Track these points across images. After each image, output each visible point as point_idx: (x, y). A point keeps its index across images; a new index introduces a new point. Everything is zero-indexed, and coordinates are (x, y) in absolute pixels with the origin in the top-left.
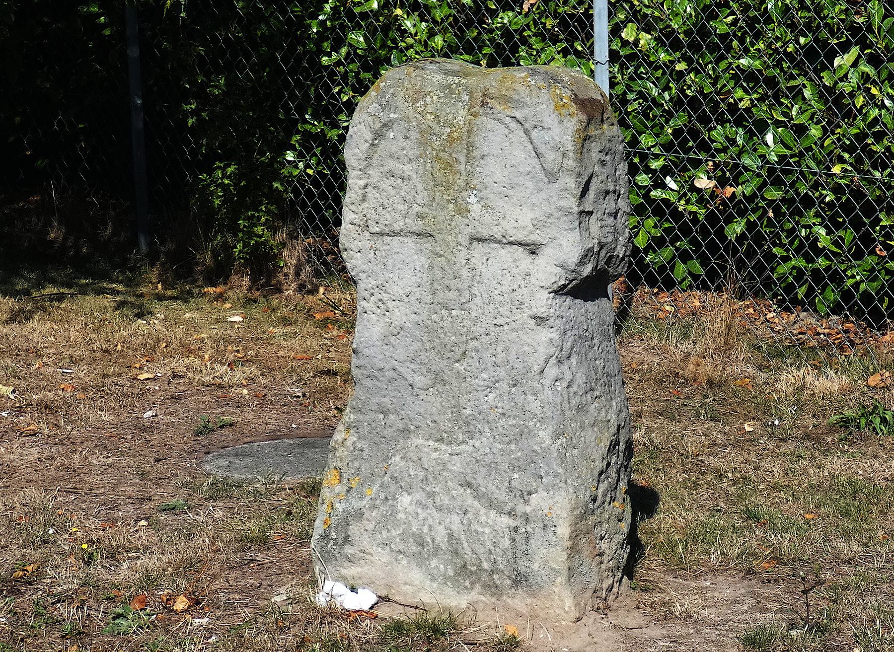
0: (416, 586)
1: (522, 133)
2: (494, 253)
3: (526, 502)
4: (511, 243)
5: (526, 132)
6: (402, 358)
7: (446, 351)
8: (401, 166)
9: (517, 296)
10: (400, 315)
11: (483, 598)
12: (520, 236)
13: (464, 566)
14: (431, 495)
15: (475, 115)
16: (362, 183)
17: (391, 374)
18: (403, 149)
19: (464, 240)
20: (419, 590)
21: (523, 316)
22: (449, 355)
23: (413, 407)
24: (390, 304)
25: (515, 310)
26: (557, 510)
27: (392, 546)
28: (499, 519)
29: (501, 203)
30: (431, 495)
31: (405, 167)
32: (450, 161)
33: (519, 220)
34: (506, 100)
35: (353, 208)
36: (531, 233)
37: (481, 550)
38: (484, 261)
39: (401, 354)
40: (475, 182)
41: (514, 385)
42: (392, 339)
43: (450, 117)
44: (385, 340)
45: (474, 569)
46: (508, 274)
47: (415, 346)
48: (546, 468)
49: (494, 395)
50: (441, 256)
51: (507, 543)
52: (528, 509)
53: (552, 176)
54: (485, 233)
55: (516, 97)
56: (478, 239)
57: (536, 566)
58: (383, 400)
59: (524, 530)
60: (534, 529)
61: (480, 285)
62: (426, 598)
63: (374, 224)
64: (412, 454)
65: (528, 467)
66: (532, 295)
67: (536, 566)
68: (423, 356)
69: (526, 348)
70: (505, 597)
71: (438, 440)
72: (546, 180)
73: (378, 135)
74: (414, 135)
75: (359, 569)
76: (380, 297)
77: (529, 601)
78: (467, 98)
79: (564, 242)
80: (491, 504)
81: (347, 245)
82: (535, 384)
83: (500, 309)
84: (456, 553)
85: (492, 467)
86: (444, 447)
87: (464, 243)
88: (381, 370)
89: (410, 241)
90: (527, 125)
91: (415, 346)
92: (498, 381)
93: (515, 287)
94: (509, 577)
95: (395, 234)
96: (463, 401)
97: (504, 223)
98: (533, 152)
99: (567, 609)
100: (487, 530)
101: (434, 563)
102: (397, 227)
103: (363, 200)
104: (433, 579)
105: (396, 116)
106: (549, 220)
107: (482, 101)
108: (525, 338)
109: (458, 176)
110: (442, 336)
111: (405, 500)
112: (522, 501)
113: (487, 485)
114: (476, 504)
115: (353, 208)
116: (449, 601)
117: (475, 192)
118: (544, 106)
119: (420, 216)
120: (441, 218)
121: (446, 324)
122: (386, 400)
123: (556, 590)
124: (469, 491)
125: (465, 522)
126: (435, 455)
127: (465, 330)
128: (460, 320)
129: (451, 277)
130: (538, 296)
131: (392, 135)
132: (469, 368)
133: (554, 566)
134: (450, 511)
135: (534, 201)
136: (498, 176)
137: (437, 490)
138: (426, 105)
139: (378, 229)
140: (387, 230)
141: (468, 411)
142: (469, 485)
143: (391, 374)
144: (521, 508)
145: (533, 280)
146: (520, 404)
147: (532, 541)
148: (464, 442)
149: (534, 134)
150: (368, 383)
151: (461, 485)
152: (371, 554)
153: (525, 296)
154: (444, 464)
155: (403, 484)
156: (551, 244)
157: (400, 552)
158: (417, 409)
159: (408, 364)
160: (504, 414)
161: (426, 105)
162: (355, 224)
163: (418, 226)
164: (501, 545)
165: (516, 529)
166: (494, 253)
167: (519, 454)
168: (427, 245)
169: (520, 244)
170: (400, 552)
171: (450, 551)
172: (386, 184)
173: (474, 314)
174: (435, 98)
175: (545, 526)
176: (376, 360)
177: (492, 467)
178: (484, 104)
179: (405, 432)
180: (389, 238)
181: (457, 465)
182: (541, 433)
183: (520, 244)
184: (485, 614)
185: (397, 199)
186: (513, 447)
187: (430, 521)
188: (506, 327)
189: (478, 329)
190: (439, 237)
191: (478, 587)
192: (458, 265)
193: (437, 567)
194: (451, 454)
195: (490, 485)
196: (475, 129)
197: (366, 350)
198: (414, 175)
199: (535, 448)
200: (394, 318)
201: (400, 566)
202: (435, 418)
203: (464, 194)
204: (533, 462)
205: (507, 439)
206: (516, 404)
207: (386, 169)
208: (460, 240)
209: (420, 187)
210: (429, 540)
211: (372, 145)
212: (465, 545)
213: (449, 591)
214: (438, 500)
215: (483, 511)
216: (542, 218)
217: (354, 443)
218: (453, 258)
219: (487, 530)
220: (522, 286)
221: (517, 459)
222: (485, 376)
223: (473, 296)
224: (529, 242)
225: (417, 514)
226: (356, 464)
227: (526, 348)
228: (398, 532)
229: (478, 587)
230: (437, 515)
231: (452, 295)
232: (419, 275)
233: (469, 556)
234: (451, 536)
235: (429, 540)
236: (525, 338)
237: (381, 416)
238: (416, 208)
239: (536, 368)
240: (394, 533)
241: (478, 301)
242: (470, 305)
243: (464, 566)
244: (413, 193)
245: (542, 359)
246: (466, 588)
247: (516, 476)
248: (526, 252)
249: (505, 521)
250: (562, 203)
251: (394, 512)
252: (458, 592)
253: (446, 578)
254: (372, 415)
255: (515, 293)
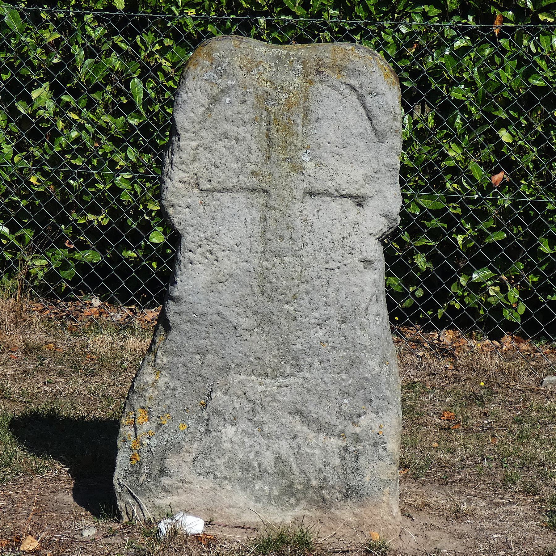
0: (241, 508)
1: (355, 99)
2: (324, 206)
3: (355, 424)
4: (343, 196)
5: (360, 98)
6: (227, 303)
7: (271, 297)
8: (235, 128)
9: (348, 242)
10: (228, 264)
11: (307, 512)
12: (352, 190)
13: (291, 485)
14: (259, 425)
15: (311, 82)
16: (194, 144)
17: (216, 318)
18: (238, 113)
19: (298, 194)
20: (243, 511)
21: (354, 261)
22: (280, 297)
23: (235, 347)
24: (220, 254)
25: (346, 255)
26: (387, 429)
27: (217, 473)
28: (328, 441)
29: (332, 161)
30: (259, 425)
31: (240, 130)
32: (281, 125)
33: (351, 175)
34: (340, 69)
35: (184, 167)
36: (362, 186)
37: (310, 470)
38: (316, 213)
39: (227, 298)
40: (309, 142)
41: (343, 322)
42: (219, 286)
43: (286, 84)
44: (212, 287)
45: (300, 487)
46: (339, 224)
47: (245, 291)
48: (376, 393)
49: (325, 331)
50: (275, 209)
51: (337, 461)
52: (358, 430)
53: (380, 136)
54: (319, 186)
55: (351, 66)
56: (311, 193)
57: (367, 479)
58: (201, 342)
59: (354, 448)
60: (364, 447)
61: (311, 234)
62: (249, 518)
63: (206, 181)
64: (235, 389)
65: (357, 393)
66: (362, 241)
67: (367, 479)
68: (250, 301)
69: (354, 289)
70: (332, 510)
71: (260, 375)
72: (375, 140)
73: (214, 100)
74: (251, 100)
75: (176, 498)
76: (208, 248)
77: (357, 510)
78: (300, 68)
79: (388, 194)
80: (322, 427)
81: (175, 201)
82: (364, 320)
83: (332, 255)
84: (283, 474)
85: (324, 395)
86: (268, 381)
87: (298, 197)
88: (203, 315)
89: (241, 197)
90: (363, 92)
91: (245, 291)
92: (328, 319)
93: (346, 235)
94: (339, 491)
95: (227, 190)
96: (292, 338)
97: (338, 178)
98: (365, 116)
99: (394, 514)
100: (317, 451)
101: (258, 485)
102: (229, 184)
103: (194, 160)
104: (257, 500)
105: (234, 83)
106: (377, 176)
107: (317, 70)
108: (354, 279)
109: (295, 137)
110: (274, 281)
111: (229, 431)
112: (350, 423)
113: (317, 410)
114: (305, 429)
115: (184, 167)
116: (273, 519)
117: (308, 151)
118: (378, 75)
119: (254, 173)
120: (277, 175)
121: (279, 269)
122: (207, 342)
123: (385, 499)
124: (298, 418)
125: (294, 446)
126: (261, 388)
127: (297, 274)
128: (292, 265)
129: (285, 227)
130: (367, 242)
131: (228, 100)
132: (300, 309)
133: (383, 477)
134: (277, 437)
135: (365, 158)
136: (332, 137)
137: (265, 419)
138: (260, 74)
139: (209, 186)
140: (219, 187)
141: (298, 346)
142: (299, 413)
143: (216, 318)
144: (350, 430)
145: (362, 228)
146: (350, 338)
147: (362, 457)
148: (291, 375)
149: (369, 99)
150: (188, 327)
151: (290, 413)
152: (192, 483)
153: (356, 242)
154: (273, 396)
155: (226, 417)
156: (377, 197)
157: (225, 478)
158: (239, 348)
159: (233, 308)
160: (334, 348)
161: (260, 74)
162: (184, 182)
163: (254, 182)
164: (331, 464)
165: (346, 449)
166: (324, 206)
167: (350, 382)
168: (259, 200)
169: (351, 197)
170: (225, 478)
171: (276, 473)
172: (219, 146)
173: (305, 260)
174: (267, 67)
175: (377, 443)
176: (199, 307)
177: (324, 395)
178: (318, 72)
179: (225, 370)
180: (219, 194)
181: (287, 396)
182: (371, 363)
183: (351, 197)
184: (337, 526)
185: (230, 158)
186: (344, 376)
187: (257, 448)
188: (337, 271)
189: (309, 273)
190: (273, 192)
191: (304, 503)
192: (293, 216)
193: (263, 489)
194: (280, 387)
195: (321, 411)
196: (311, 95)
197: (190, 297)
198: (248, 137)
199: (366, 375)
200: (223, 267)
201: (224, 492)
202: (259, 355)
203: (300, 153)
204: (363, 388)
205: (337, 370)
206: (346, 338)
207: (220, 131)
208: (295, 193)
209: (254, 147)
210: (256, 465)
211: (208, 109)
212: (294, 466)
213: (273, 509)
214: (266, 428)
215: (312, 435)
216: (370, 174)
217: (167, 383)
218: (288, 211)
219: (317, 451)
220: (353, 234)
221: (348, 387)
222: (316, 315)
223: (305, 244)
224: (360, 195)
225: (243, 443)
226: (168, 402)
227: (354, 289)
228: (223, 461)
229: (304, 503)
230: (264, 442)
231: (285, 244)
232: (250, 227)
233: (297, 476)
234: (278, 459)
235: (256, 465)
236: (354, 279)
237: (198, 357)
238: (250, 167)
239: (363, 305)
240: (218, 461)
241: (309, 248)
242: (301, 252)
243: (291, 485)
244: (247, 153)
245: (368, 297)
246: (291, 505)
247: (346, 401)
248: (354, 204)
249: (334, 442)
250: (388, 161)
251: (219, 442)
252: (283, 510)
253: (270, 497)
254: (189, 357)
255: (346, 240)
